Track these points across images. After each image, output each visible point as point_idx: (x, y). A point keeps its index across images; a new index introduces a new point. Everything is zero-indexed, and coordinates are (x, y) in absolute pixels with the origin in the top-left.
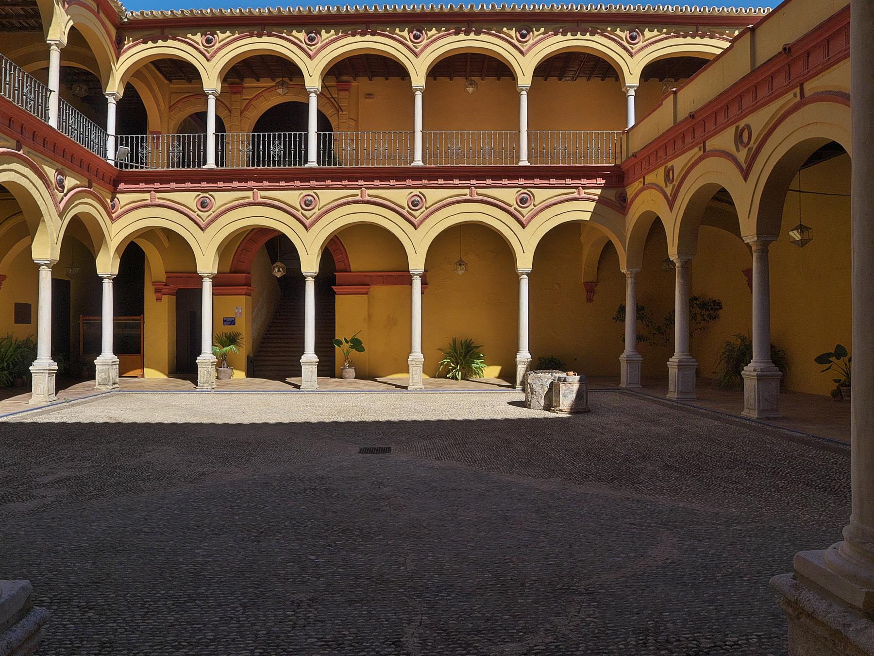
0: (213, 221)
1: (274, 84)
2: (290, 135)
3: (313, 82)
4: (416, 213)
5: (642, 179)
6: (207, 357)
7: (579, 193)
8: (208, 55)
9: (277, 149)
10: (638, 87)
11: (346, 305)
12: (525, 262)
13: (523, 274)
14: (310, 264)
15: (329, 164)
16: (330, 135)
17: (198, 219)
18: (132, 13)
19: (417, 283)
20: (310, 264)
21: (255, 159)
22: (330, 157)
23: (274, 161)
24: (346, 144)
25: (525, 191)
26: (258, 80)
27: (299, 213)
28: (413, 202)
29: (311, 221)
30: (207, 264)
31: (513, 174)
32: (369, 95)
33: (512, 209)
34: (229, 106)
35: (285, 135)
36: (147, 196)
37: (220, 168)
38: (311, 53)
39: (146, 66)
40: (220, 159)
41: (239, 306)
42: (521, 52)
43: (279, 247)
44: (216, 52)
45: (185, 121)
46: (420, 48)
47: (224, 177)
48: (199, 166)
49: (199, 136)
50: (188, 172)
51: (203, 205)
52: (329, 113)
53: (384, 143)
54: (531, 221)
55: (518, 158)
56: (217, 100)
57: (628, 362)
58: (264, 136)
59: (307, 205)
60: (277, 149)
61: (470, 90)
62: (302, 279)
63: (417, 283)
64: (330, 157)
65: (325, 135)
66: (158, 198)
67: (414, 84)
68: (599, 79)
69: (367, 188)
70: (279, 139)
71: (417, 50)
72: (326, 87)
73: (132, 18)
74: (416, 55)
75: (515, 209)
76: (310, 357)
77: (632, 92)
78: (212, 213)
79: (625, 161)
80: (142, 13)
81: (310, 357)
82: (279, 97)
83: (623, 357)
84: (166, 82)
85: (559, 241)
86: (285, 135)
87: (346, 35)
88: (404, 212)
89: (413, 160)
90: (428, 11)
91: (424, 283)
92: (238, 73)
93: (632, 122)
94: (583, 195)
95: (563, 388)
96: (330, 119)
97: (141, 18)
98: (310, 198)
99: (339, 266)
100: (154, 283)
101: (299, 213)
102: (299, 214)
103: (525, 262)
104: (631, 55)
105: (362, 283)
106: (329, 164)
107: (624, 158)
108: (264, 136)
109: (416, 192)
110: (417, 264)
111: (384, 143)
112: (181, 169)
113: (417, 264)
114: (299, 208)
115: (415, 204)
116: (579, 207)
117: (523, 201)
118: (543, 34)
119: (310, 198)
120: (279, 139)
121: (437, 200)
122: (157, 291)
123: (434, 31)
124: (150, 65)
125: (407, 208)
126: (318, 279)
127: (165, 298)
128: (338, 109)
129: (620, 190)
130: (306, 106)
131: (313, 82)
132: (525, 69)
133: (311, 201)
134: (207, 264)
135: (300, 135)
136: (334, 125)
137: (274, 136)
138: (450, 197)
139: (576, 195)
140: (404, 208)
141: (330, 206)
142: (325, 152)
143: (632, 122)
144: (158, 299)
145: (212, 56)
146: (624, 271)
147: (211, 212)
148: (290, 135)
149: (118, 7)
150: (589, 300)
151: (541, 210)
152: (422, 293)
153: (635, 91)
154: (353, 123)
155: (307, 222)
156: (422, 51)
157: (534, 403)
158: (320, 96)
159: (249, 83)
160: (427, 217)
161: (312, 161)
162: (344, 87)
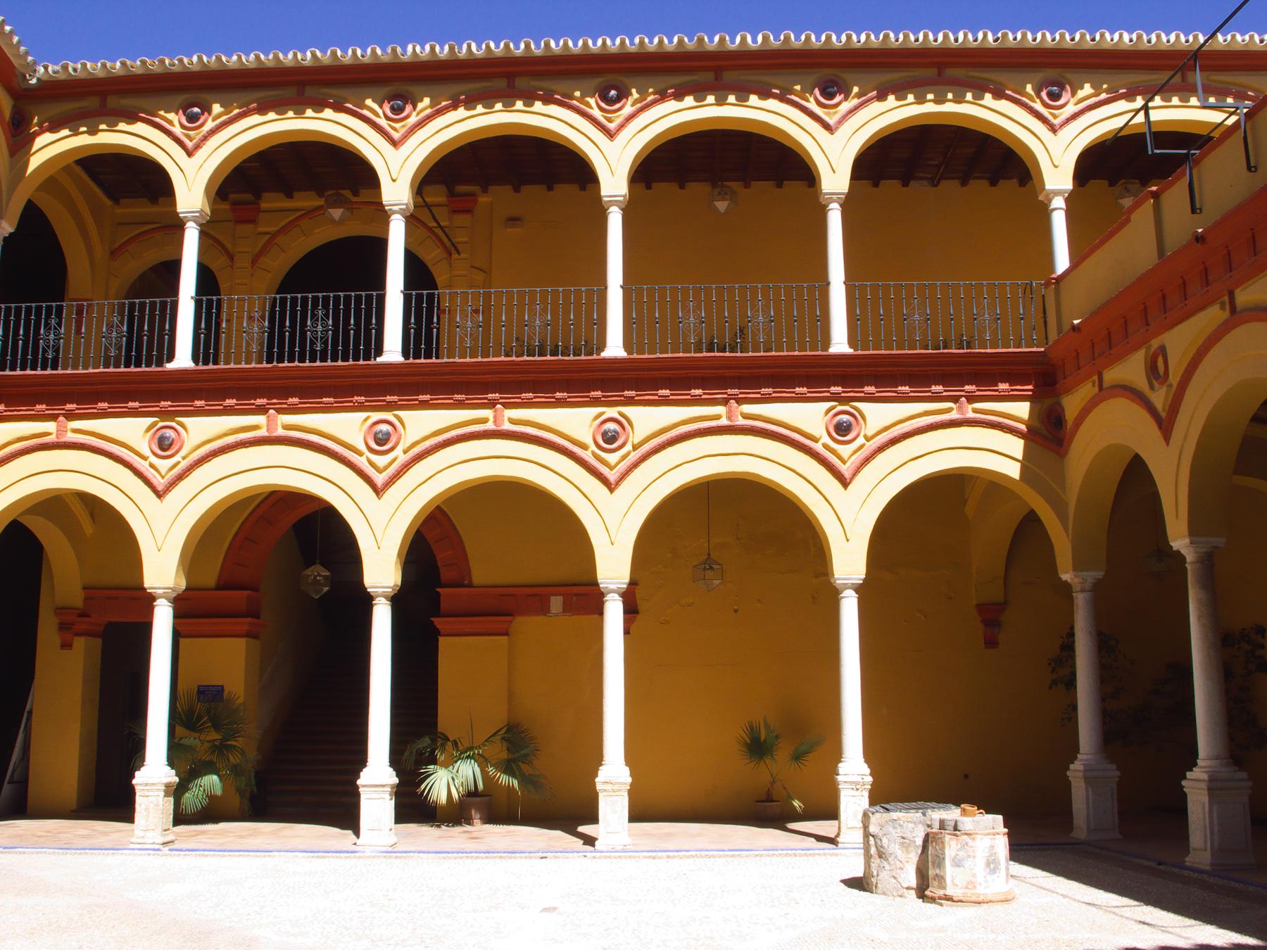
0: (180, 477)
1: (321, 202)
2: (348, 298)
3: (396, 191)
4: (612, 458)
5: (1096, 378)
6: (154, 774)
7: (960, 409)
8: (190, 144)
9: (319, 327)
10: (1072, 193)
11: (457, 656)
12: (849, 561)
13: (846, 587)
14: (381, 570)
15: (356, 358)
16: (431, 297)
17: (150, 473)
18: (46, 68)
19: (614, 612)
20: (381, 570)
21: (275, 348)
22: (303, 345)
23: (45, 360)
24: (532, 313)
25: (846, 408)
26: (290, 196)
27: (363, 459)
28: (604, 434)
29: (382, 478)
30: (162, 570)
31: (816, 376)
32: (514, 220)
33: (818, 447)
34: (229, 246)
35: (337, 299)
36: (50, 426)
37: (201, 367)
38: (396, 136)
39: (67, 169)
40: (205, 347)
41: (231, 662)
42: (827, 127)
43: (314, 533)
44: (205, 138)
45: (142, 277)
46: (403, 131)
47: (206, 390)
48: (160, 364)
49: (369, 298)
50: (139, 381)
51: (842, 430)
52: (431, 256)
53: (544, 310)
54: (852, 473)
55: (827, 342)
56: (203, 234)
57: (1089, 780)
58: (294, 300)
59: (380, 442)
60: (319, 327)
61: (722, 206)
62: (366, 601)
63: (614, 612)
64: (303, 345)
65: (419, 297)
66: (511, 416)
67: (1049, 186)
68: (509, 188)
69: (506, 406)
70: (326, 306)
71: (612, 126)
72: (428, 206)
73: (45, 78)
74: (611, 135)
75: (826, 446)
76: (377, 776)
77: (1059, 203)
78: (181, 460)
79: (1056, 342)
80: (65, 68)
81: (377, 776)
82: (336, 223)
83: (1076, 769)
84: (108, 202)
85: (925, 518)
86: (337, 299)
87: (663, 97)
88: (587, 455)
89: (602, 345)
90: (633, 49)
91: (631, 610)
92: (242, 183)
93: (1062, 261)
94: (970, 415)
95: (952, 847)
96: (433, 270)
97: (62, 76)
98: (845, 417)
99: (445, 575)
100: (60, 610)
101: (363, 459)
102: (362, 462)
103: (849, 561)
104: (1053, 129)
105: (501, 609)
106: (356, 358)
107: (1053, 335)
108: (358, 298)
109: (612, 412)
110: (613, 566)
111: (766, 309)
112: (340, 363)
113: (613, 566)
114: (363, 448)
115: (610, 438)
116: (986, 442)
117: (842, 430)
118: (859, 95)
119: (845, 417)
120: (326, 306)
121: (205, 438)
122: (64, 627)
123: (1087, 89)
124: (78, 170)
125: (593, 447)
126: (398, 601)
127: (80, 643)
128: (451, 249)
129: (1049, 402)
130: (380, 246)
131: (396, 191)
132: (1056, 161)
133: (388, 435)
134: (162, 570)
135: (369, 298)
136: (440, 280)
137: (315, 300)
138: (226, 435)
139: (955, 415)
140: (360, 454)
141: (428, 444)
142: (419, 337)
143: (1062, 261)
144: (66, 645)
145: (197, 147)
146: (1066, 577)
147: (178, 458)
148: (348, 298)
149: (18, 56)
150: (991, 643)
151: (881, 449)
152: (627, 632)
153: (1067, 200)
154: (479, 277)
155: (380, 479)
156: (622, 127)
157: (883, 878)
158: (412, 220)
159: (271, 201)
160: (635, 465)
161: (392, 351)
162: (461, 205)
